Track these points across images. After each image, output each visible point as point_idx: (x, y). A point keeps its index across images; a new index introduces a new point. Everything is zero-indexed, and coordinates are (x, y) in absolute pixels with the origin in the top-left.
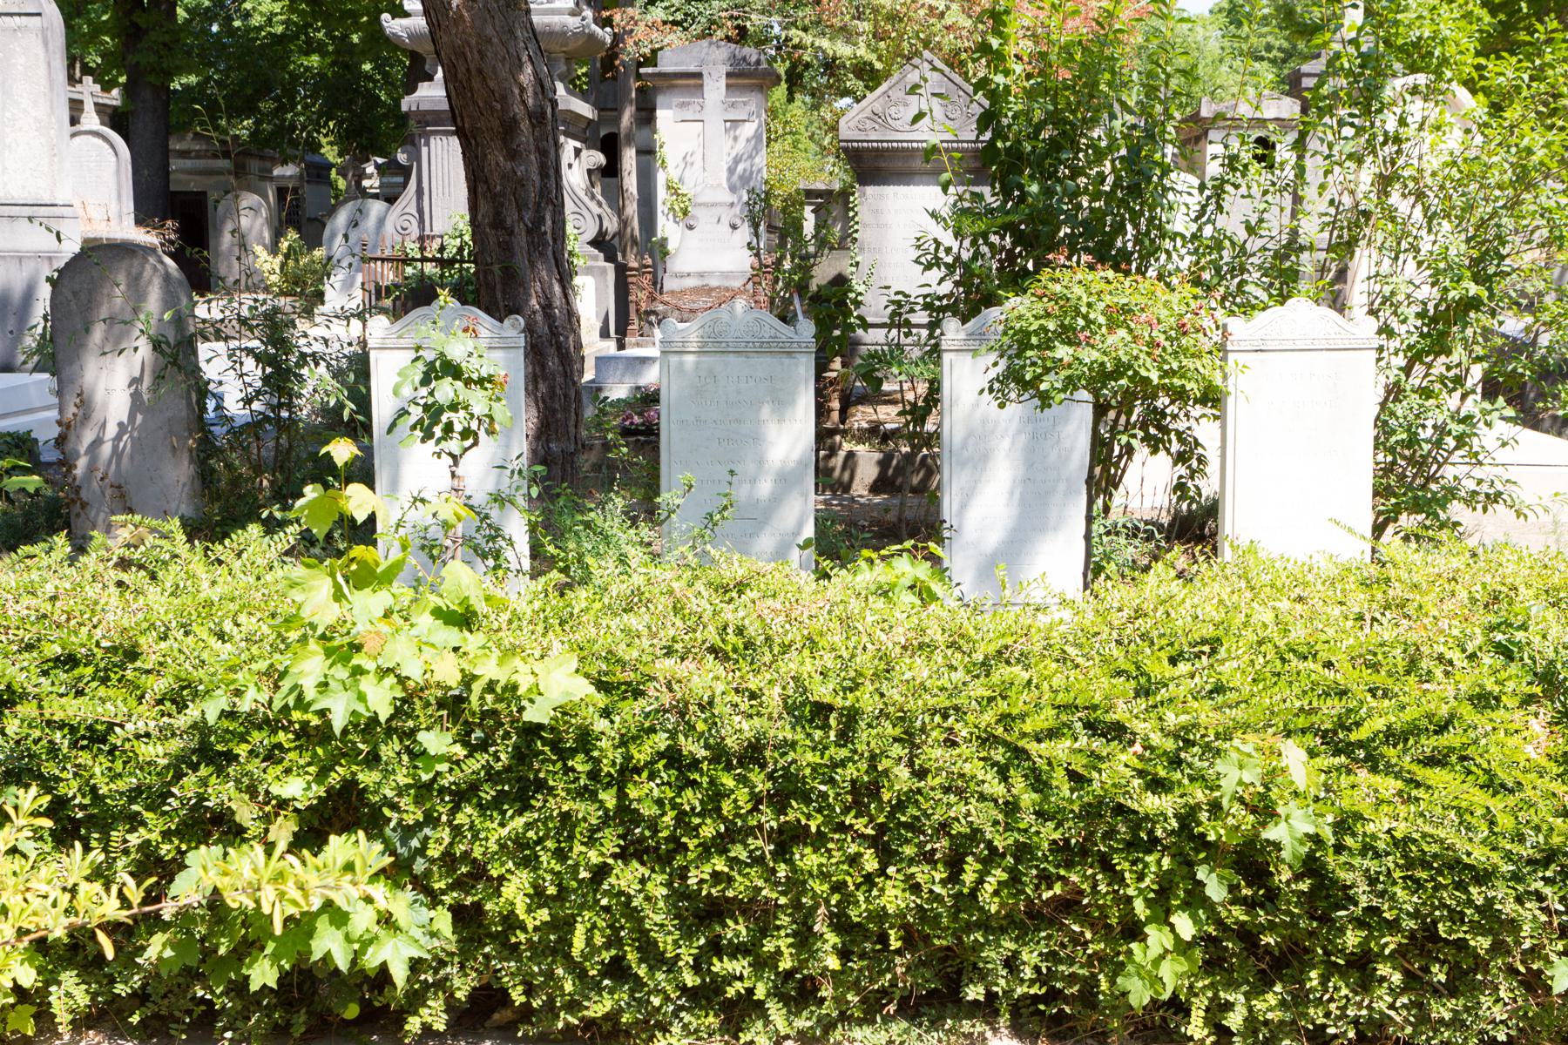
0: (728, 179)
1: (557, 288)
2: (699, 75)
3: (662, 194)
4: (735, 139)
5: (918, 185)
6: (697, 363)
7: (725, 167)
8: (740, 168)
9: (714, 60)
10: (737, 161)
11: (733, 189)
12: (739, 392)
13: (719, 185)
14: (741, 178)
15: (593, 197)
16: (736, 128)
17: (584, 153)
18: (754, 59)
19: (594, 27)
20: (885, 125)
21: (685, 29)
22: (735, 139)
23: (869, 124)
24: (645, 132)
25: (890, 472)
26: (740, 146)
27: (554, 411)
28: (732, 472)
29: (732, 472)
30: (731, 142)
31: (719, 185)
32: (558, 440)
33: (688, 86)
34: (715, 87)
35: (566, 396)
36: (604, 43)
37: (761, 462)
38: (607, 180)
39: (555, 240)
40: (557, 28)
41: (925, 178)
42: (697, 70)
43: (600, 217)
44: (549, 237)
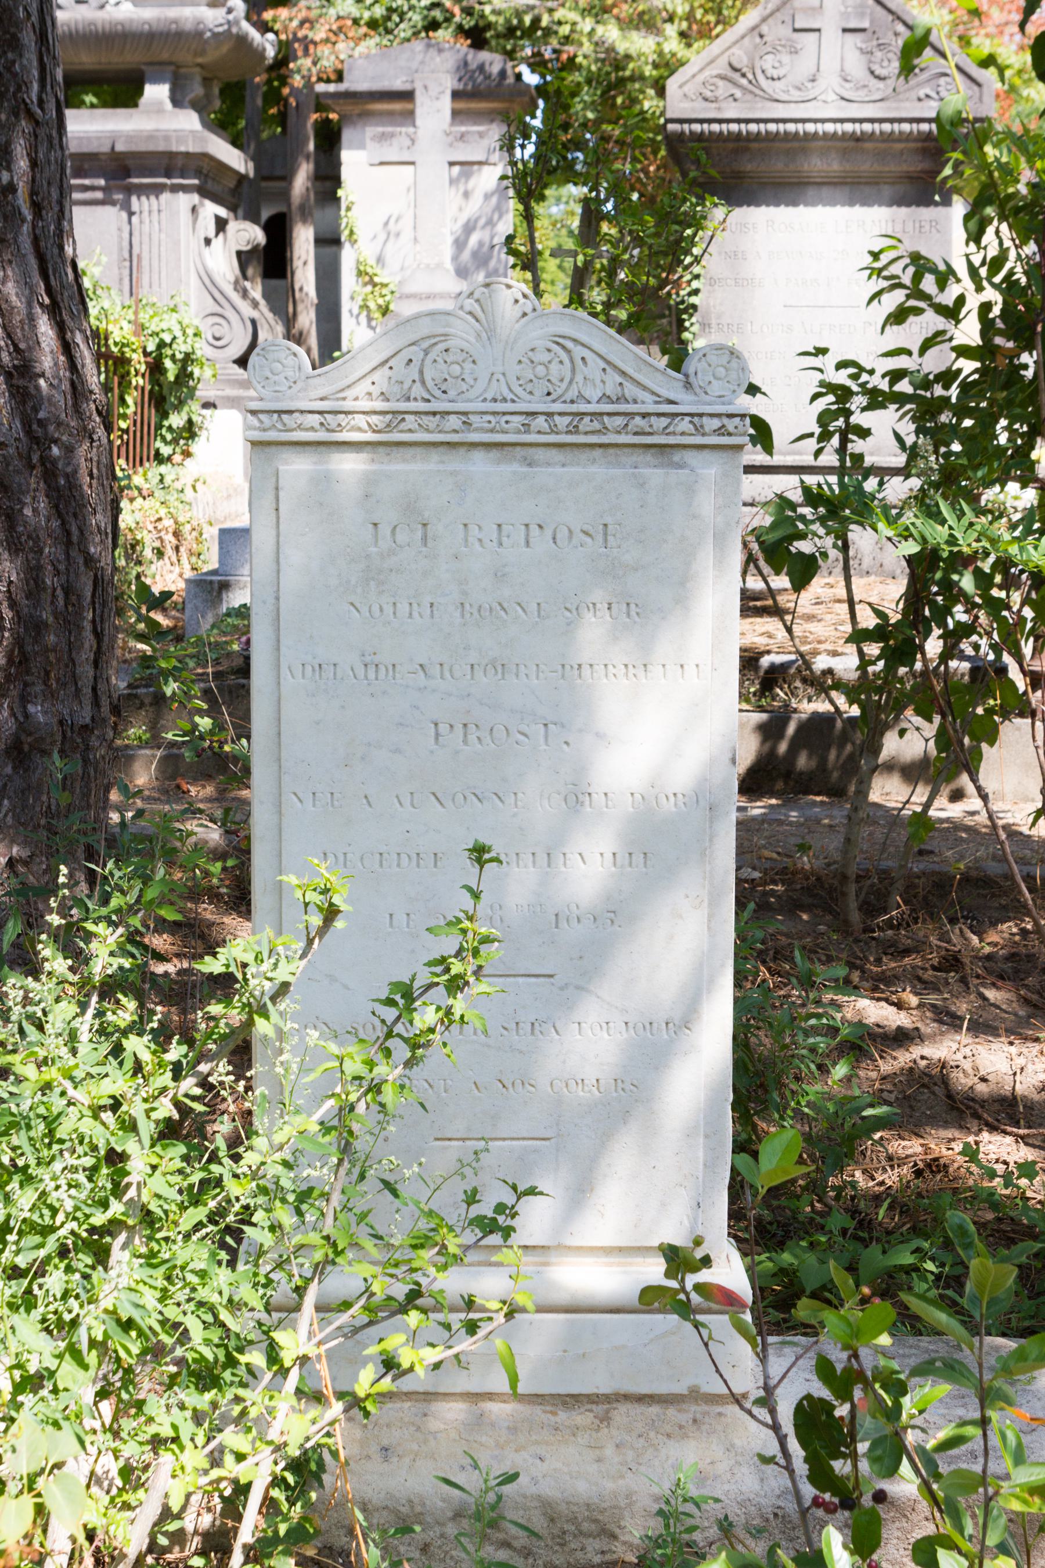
0: (455, 258)
1: (45, 328)
2: (408, 96)
3: (349, 282)
4: (466, 195)
5: (813, 204)
6: (370, 481)
7: (450, 240)
8: (474, 239)
9: (432, 71)
10: (469, 228)
11: (462, 272)
12: (500, 576)
13: (439, 265)
14: (475, 254)
15: (245, 294)
16: (467, 176)
17: (233, 226)
18: (495, 69)
19: (246, 27)
20: (754, 90)
21: (388, 32)
22: (466, 195)
23: (723, 89)
24: (329, 211)
25: (783, 747)
26: (474, 206)
27: (38, 628)
28: (480, 853)
29: (480, 853)
30: (459, 199)
31: (439, 265)
32: (51, 695)
33: (391, 113)
34: (434, 110)
35: (68, 591)
36: (261, 54)
37: (576, 797)
38: (274, 282)
39: (37, 208)
40: (188, 26)
41: (825, 191)
42: (407, 87)
43: (254, 322)
44: (22, 198)
